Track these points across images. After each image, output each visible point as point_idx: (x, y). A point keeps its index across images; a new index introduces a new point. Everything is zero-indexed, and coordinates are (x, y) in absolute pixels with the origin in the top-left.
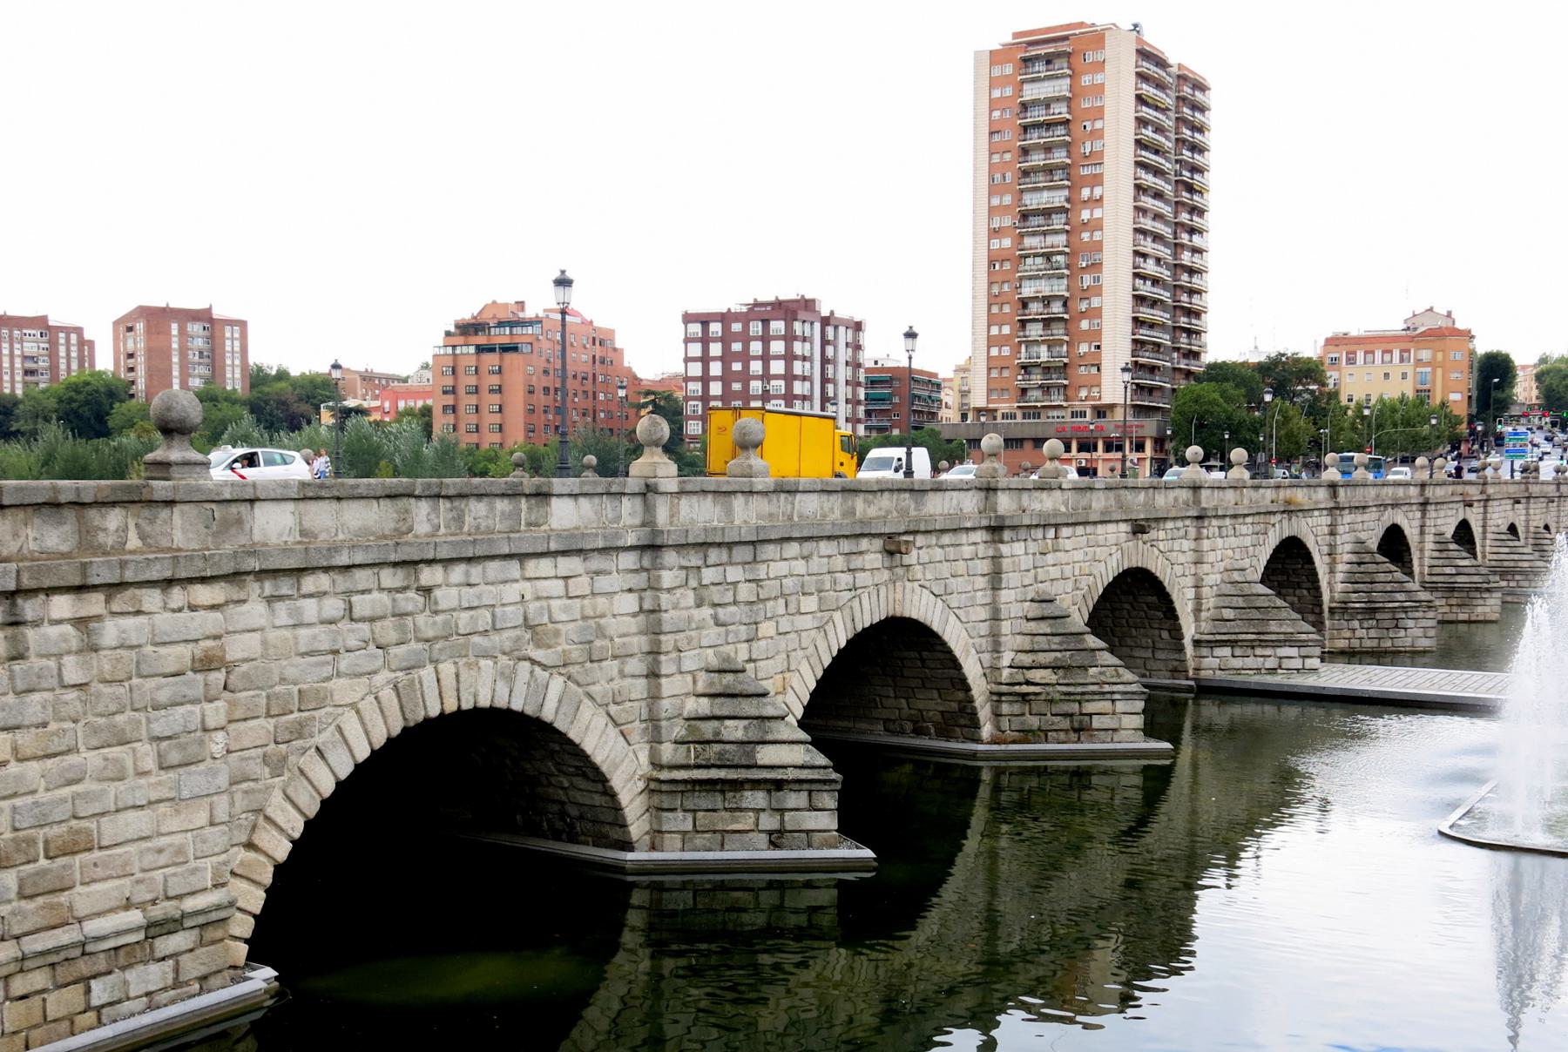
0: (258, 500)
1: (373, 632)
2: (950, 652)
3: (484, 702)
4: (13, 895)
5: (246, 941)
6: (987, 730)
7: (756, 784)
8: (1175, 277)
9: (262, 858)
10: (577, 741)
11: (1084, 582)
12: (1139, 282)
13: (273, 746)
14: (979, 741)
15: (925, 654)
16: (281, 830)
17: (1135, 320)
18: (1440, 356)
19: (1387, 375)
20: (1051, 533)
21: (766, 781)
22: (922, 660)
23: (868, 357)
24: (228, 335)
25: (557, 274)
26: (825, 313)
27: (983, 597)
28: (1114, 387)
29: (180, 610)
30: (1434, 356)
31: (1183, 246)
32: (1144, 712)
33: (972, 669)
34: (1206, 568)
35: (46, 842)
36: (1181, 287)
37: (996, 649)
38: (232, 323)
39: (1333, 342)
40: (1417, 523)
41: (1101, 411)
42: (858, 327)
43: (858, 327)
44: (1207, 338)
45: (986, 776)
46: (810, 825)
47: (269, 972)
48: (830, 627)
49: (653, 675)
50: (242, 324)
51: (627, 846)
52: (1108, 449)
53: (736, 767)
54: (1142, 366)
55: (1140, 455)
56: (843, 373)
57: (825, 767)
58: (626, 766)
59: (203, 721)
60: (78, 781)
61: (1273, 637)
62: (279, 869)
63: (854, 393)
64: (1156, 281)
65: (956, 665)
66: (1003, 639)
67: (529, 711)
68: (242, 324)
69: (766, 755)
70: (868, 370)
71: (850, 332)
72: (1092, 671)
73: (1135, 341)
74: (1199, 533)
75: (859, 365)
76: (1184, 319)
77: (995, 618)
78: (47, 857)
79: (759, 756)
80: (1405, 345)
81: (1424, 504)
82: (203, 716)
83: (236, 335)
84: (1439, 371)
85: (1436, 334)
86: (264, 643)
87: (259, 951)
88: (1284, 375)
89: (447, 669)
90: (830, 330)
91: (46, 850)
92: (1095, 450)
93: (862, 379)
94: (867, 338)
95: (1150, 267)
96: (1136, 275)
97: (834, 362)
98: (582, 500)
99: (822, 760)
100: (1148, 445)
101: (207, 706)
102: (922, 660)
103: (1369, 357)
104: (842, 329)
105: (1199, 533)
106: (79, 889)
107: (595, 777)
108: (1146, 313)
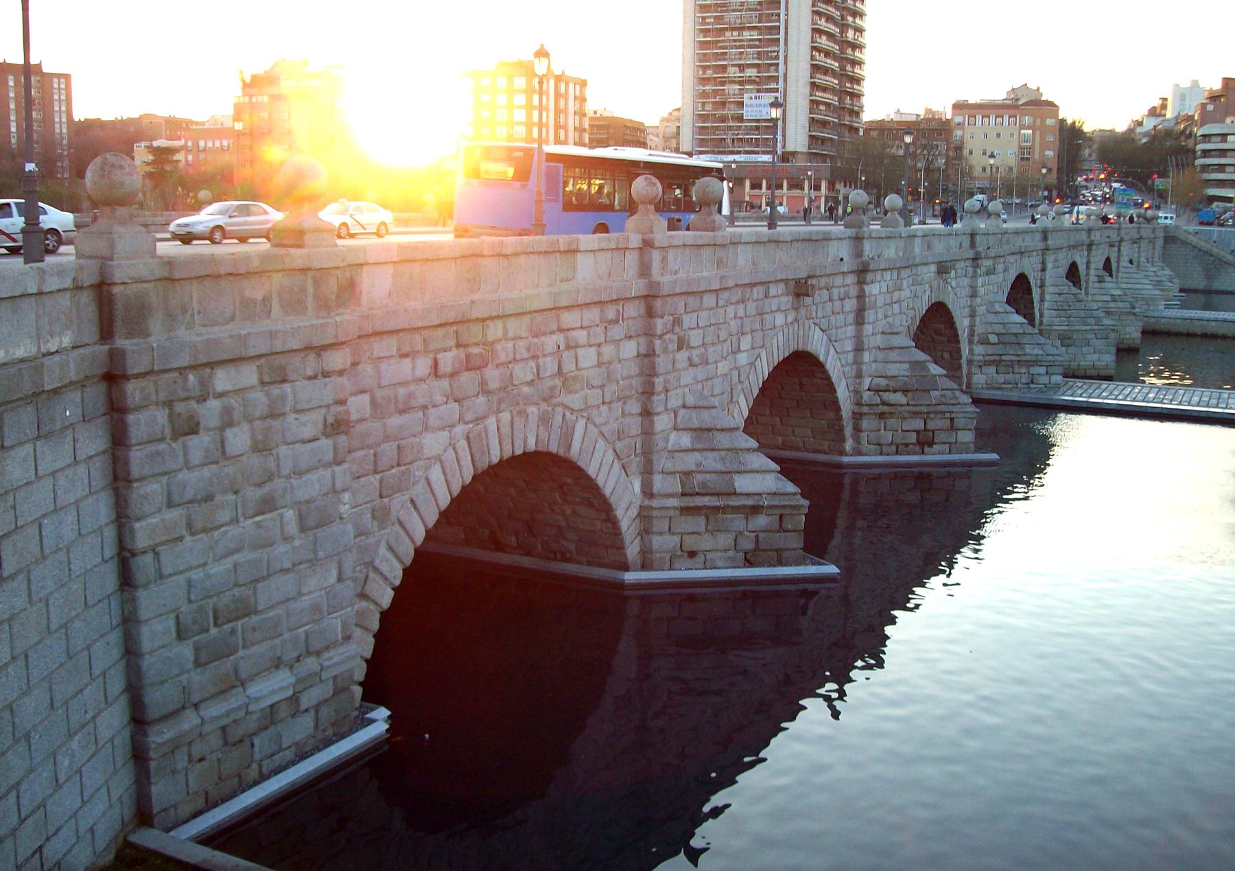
0: (367, 264)
1: (451, 387)
2: (828, 378)
3: (532, 446)
4: (191, 665)
5: (361, 684)
6: (849, 445)
7: (737, 509)
8: (842, 51)
9: (372, 607)
10: (594, 477)
11: (911, 313)
12: (816, 54)
13: (379, 501)
14: (842, 453)
15: (804, 380)
16: (386, 578)
17: (813, 84)
18: (1038, 122)
19: (998, 135)
20: (895, 273)
21: (744, 507)
22: (801, 385)
23: (590, 108)
24: (56, 86)
25: (538, 48)
26: (558, 72)
27: (851, 330)
28: (796, 138)
29: (315, 377)
30: (1034, 122)
31: (848, 26)
32: (976, 429)
33: (843, 393)
34: (978, 300)
35: (215, 612)
36: (847, 59)
37: (859, 375)
38: (59, 76)
39: (959, 107)
40: (1085, 260)
41: (787, 157)
42: (583, 84)
43: (583, 84)
44: (865, 101)
45: (847, 480)
46: (781, 545)
47: (382, 713)
48: (758, 363)
49: (647, 413)
50: (67, 77)
51: (625, 567)
52: (790, 187)
53: (718, 494)
54: (818, 121)
55: (817, 193)
56: (572, 121)
57: (794, 494)
58: (623, 492)
59: (334, 484)
60: (237, 551)
61: (1028, 358)
62: (385, 616)
63: (581, 137)
64: (827, 54)
65: (833, 390)
66: (864, 367)
67: (562, 453)
68: (67, 77)
69: (743, 484)
70: (591, 119)
71: (578, 87)
72: (934, 394)
73: (812, 102)
74: (975, 272)
75: (585, 115)
76: (848, 85)
77: (859, 349)
78: (216, 625)
79: (737, 485)
80: (1012, 112)
81: (1090, 246)
82: (333, 477)
83: (63, 86)
84: (1038, 133)
85: (1028, 105)
86: (374, 403)
87: (374, 691)
88: (931, 131)
89: (506, 417)
90: (563, 86)
91: (216, 618)
92: (761, 188)
93: (587, 126)
94: (589, 93)
95: (824, 41)
96: (814, 48)
97: (566, 111)
98: (599, 254)
99: (791, 487)
100: (824, 185)
101: (337, 469)
102: (801, 385)
103: (999, 120)
104: (571, 86)
105: (975, 272)
106: (241, 653)
107: (604, 508)
108: (821, 79)
